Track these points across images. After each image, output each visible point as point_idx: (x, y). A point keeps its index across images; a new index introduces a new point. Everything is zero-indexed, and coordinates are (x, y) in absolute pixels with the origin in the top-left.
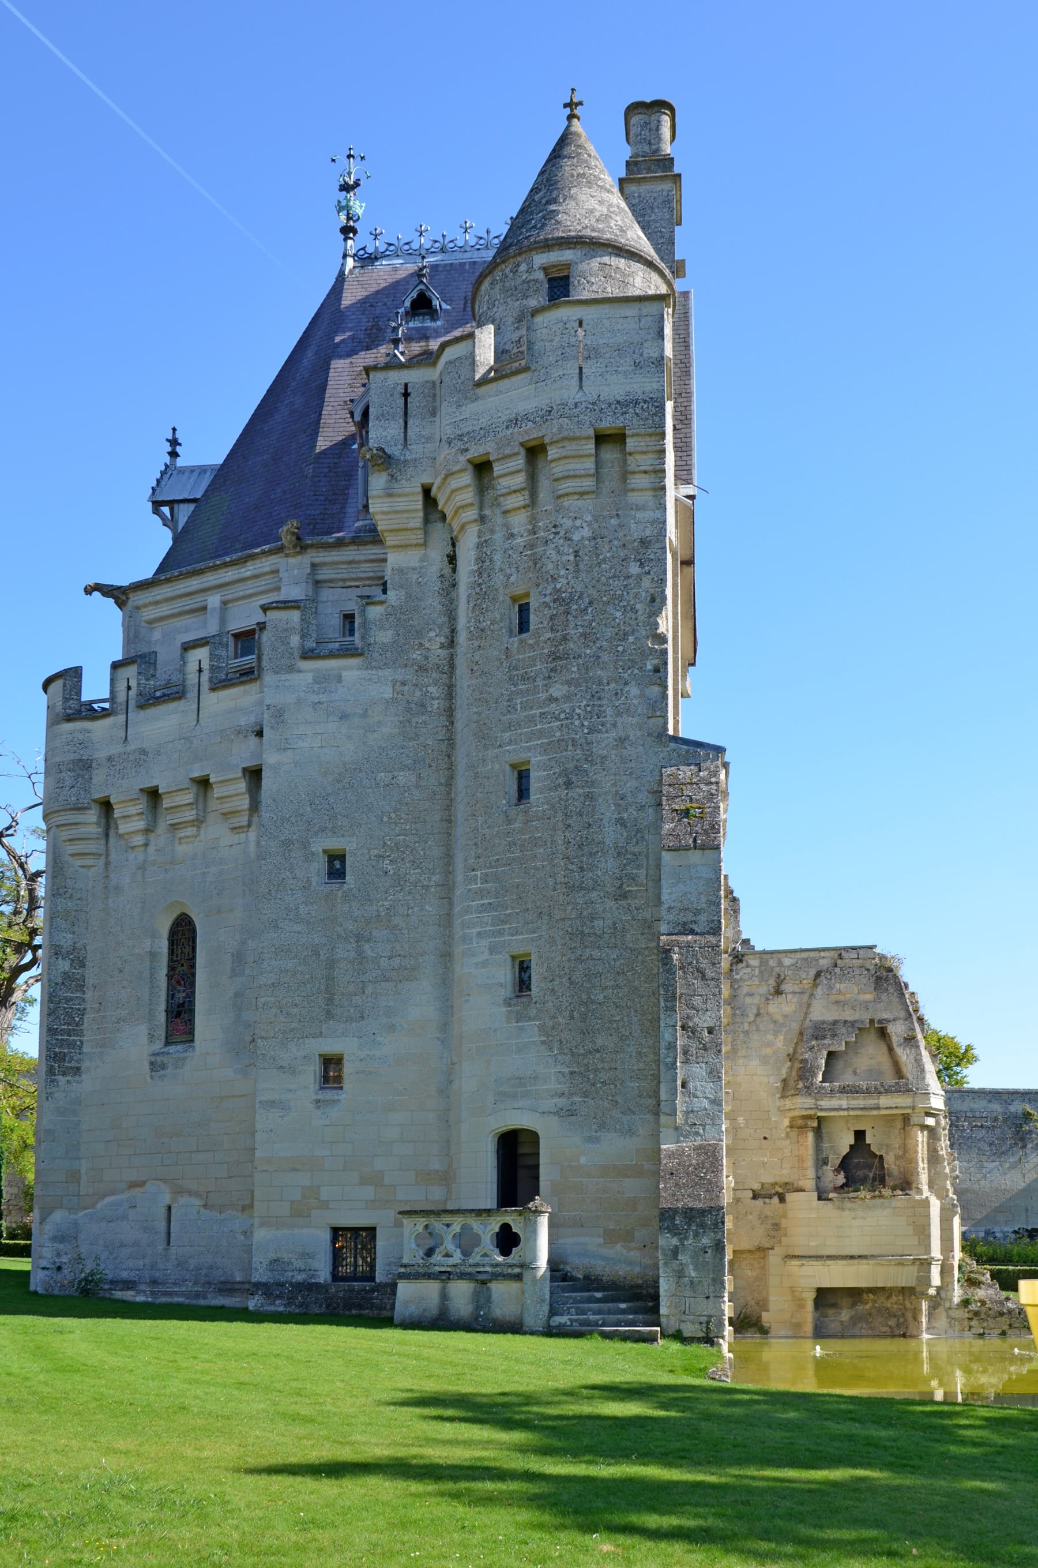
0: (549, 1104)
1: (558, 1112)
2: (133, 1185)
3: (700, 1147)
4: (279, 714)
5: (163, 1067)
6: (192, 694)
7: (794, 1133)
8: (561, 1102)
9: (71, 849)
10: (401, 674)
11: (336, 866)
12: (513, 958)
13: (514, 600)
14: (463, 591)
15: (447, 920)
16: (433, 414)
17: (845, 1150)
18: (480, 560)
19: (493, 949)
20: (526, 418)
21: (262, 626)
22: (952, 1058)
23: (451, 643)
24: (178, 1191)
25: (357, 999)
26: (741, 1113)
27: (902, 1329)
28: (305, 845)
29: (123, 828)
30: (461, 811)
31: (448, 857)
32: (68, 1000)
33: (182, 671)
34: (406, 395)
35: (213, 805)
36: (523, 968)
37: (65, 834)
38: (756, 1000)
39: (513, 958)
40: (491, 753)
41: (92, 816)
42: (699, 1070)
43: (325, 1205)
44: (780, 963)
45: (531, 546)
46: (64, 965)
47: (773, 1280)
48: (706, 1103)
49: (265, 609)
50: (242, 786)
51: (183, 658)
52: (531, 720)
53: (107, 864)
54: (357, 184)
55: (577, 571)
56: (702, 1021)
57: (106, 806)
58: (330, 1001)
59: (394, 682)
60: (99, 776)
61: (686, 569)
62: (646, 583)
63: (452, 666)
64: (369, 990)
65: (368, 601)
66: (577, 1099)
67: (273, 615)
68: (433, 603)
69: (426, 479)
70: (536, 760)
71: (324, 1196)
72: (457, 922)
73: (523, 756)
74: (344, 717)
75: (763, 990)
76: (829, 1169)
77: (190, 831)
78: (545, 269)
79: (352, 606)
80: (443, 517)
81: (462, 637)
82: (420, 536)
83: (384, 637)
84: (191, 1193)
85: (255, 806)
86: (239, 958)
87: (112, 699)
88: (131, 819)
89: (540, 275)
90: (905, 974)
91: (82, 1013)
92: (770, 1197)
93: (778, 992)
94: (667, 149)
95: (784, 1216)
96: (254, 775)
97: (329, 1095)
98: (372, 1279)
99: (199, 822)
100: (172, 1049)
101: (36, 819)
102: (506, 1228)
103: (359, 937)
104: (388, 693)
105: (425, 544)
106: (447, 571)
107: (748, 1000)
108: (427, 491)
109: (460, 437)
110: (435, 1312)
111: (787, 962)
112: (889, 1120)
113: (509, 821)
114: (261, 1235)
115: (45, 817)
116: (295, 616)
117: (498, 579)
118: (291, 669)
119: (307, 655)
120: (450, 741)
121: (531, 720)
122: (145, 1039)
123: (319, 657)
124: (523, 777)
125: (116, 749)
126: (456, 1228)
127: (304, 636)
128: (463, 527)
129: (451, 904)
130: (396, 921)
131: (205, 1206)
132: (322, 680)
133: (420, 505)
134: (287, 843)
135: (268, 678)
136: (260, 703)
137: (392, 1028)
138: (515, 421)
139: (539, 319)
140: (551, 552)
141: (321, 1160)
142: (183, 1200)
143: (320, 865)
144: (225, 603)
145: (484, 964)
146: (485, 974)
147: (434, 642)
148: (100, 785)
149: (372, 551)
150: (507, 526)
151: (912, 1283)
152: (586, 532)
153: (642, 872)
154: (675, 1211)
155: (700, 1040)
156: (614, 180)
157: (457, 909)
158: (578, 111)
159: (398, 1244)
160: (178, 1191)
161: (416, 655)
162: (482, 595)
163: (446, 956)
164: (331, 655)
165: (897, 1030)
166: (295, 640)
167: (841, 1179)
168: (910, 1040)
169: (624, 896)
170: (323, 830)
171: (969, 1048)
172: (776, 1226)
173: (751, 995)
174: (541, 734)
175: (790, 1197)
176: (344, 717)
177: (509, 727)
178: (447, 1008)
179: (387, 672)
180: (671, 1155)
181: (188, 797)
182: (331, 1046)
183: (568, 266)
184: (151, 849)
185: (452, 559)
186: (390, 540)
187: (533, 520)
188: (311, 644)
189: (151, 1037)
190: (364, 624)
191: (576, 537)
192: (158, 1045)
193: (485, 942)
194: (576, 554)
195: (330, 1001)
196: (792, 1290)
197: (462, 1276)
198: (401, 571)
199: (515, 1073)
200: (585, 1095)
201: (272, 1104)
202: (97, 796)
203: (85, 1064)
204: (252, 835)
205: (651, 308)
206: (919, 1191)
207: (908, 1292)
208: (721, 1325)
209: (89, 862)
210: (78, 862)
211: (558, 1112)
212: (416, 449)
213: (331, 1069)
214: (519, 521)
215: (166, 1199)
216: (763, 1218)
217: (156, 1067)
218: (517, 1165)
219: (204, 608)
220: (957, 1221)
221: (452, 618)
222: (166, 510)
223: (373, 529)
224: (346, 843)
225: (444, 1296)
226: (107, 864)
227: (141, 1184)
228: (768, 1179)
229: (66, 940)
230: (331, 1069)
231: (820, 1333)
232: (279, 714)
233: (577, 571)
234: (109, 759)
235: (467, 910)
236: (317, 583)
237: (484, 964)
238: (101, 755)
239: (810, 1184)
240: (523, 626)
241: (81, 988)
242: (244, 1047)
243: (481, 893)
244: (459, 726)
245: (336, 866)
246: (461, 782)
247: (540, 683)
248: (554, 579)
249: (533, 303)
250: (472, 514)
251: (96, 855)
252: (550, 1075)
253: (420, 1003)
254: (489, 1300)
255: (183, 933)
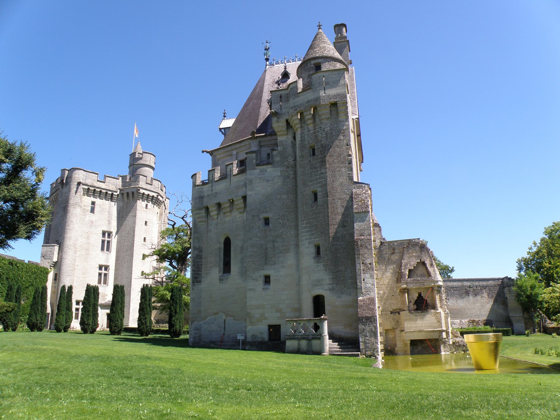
0: (327, 287)
1: (329, 290)
2: (215, 314)
3: (369, 298)
4: (251, 181)
5: (223, 280)
6: (229, 177)
7: (401, 294)
8: (330, 286)
9: (198, 220)
10: (282, 169)
11: (267, 221)
12: (315, 245)
13: (311, 147)
14: (297, 145)
15: (297, 235)
16: (288, 101)
17: (416, 298)
18: (301, 137)
19: (309, 243)
20: (311, 101)
21: (246, 158)
22: (446, 271)
23: (295, 160)
24: (227, 315)
25: (273, 259)
26: (376, 286)
27: (437, 351)
28: (258, 216)
29: (212, 214)
30: (300, 205)
31: (297, 218)
32: (198, 262)
33: (226, 171)
34: (281, 97)
35: (235, 207)
36: (318, 248)
37: (197, 216)
38: (388, 255)
39: (315, 245)
40: (307, 188)
41: (203, 211)
42: (368, 276)
43: (266, 319)
44: (394, 245)
45: (314, 133)
46: (197, 252)
47: (397, 338)
48: (370, 285)
49: (247, 153)
50: (242, 201)
51: (226, 168)
52: (317, 179)
53: (208, 224)
54: (269, 48)
55: (327, 139)
56: (368, 261)
57: (207, 209)
58: (266, 260)
59: (281, 171)
60: (205, 200)
61: (359, 137)
62: (345, 141)
63: (295, 166)
64: (277, 256)
65: (273, 150)
66: (334, 285)
67: (249, 155)
68: (290, 150)
69: (287, 118)
70: (319, 190)
71: (266, 316)
72: (300, 236)
73: (315, 189)
74: (268, 181)
75: (390, 252)
76: (412, 304)
77: (229, 214)
78: (314, 64)
79: (269, 152)
80: (292, 127)
81: (298, 158)
82: (286, 132)
83: (277, 159)
84: (230, 316)
85: (245, 206)
86: (242, 248)
87: (208, 180)
88: (214, 212)
89: (313, 66)
90: (429, 246)
91: (201, 265)
92: (396, 313)
93: (393, 253)
94: (345, 34)
95: (400, 319)
96: (245, 198)
97: (267, 286)
98: (280, 340)
99: (231, 211)
100: (225, 275)
101: (190, 214)
102: (315, 324)
103: (273, 241)
104: (279, 174)
105: (287, 134)
106: (293, 141)
107: (385, 255)
108: (287, 121)
109: (295, 107)
110: (297, 349)
111: (395, 244)
112: (428, 289)
113: (312, 207)
114: (249, 328)
115: (192, 212)
116: (254, 155)
117: (306, 142)
118: (254, 169)
119: (258, 165)
120: (296, 186)
121: (317, 179)
122: (218, 272)
123: (261, 165)
124: (315, 195)
125: (210, 193)
126: (302, 324)
127: (256, 160)
128: (297, 130)
129: (298, 231)
130: (283, 236)
131: (234, 319)
132: (262, 171)
133: (285, 124)
134: (253, 216)
135: (248, 172)
136: (246, 178)
137: (283, 267)
138: (308, 102)
139: (313, 76)
140: (320, 134)
141: (266, 305)
142: (229, 318)
143: (262, 222)
144: (237, 153)
145: (308, 247)
146: (308, 250)
147: (291, 159)
148: (206, 202)
149: (274, 137)
150: (308, 128)
151: (437, 337)
152: (329, 129)
153: (349, 219)
154: (363, 317)
155: (368, 267)
156: (331, 42)
157: (300, 232)
158: (321, 27)
159: (287, 329)
160: (227, 315)
161: (286, 163)
162: (303, 146)
163: (297, 246)
164: (264, 165)
165: (428, 262)
166: (254, 161)
167: (415, 307)
168: (432, 265)
169: (344, 226)
170: (263, 212)
171: (453, 267)
172: (398, 322)
173: (386, 254)
174: (319, 183)
175: (401, 313)
176: (268, 181)
177: (311, 182)
178: (298, 260)
179: (279, 168)
180: (361, 301)
181: (228, 205)
182: (267, 272)
183: (320, 63)
184: (219, 219)
185: (294, 138)
186: (278, 134)
187: (315, 126)
188: (258, 162)
189: (219, 271)
190: (272, 156)
191: (326, 130)
192: (221, 274)
193: (307, 241)
194: (326, 134)
195: (266, 260)
196: (403, 341)
197: (304, 338)
198: (281, 142)
199: (315, 278)
200: (337, 284)
201: (251, 290)
202: (204, 206)
203: (202, 280)
204: (245, 214)
205: (342, 72)
206: (438, 310)
207: (437, 340)
208: (377, 351)
209: (203, 223)
210: (200, 224)
211: (329, 290)
212: (284, 110)
213: (267, 280)
214: (311, 127)
215: (224, 317)
216: (394, 319)
217: (221, 280)
218: (319, 305)
219: (232, 155)
220: (449, 319)
221: (295, 153)
222: (223, 130)
223: (274, 131)
224: (269, 215)
225: (299, 345)
226: (208, 224)
227: (217, 314)
228: (395, 308)
229: (197, 245)
230: (267, 280)
231: (412, 353)
232: (251, 181)
233: (327, 139)
234: (208, 195)
235: (302, 232)
236: (261, 146)
237: (308, 247)
238: (206, 194)
239: (406, 309)
240: (314, 154)
241: (201, 258)
242: (244, 274)
243: (306, 228)
244: (298, 182)
245: (267, 221)
246: (299, 197)
247: (319, 169)
248: (321, 141)
249: (312, 72)
250: (299, 126)
251: (205, 222)
252: (326, 278)
253: (290, 259)
254: (311, 345)
255: (227, 243)
